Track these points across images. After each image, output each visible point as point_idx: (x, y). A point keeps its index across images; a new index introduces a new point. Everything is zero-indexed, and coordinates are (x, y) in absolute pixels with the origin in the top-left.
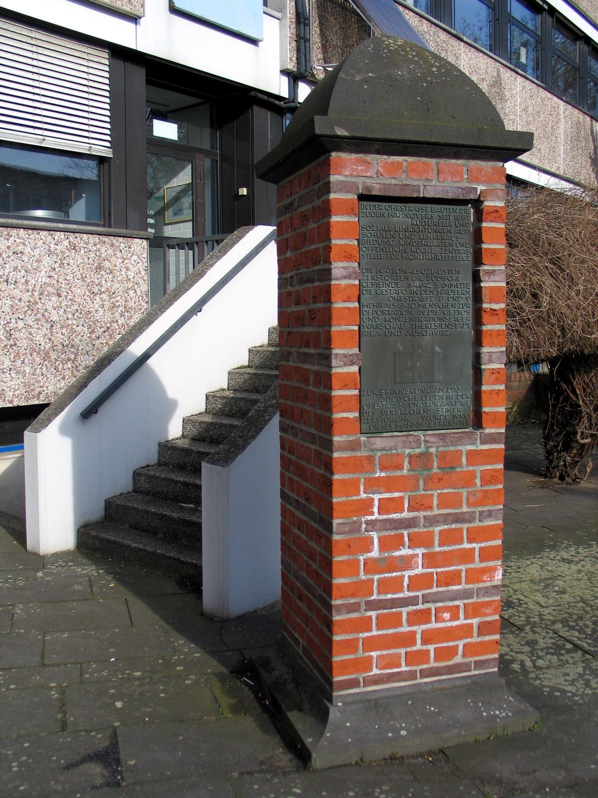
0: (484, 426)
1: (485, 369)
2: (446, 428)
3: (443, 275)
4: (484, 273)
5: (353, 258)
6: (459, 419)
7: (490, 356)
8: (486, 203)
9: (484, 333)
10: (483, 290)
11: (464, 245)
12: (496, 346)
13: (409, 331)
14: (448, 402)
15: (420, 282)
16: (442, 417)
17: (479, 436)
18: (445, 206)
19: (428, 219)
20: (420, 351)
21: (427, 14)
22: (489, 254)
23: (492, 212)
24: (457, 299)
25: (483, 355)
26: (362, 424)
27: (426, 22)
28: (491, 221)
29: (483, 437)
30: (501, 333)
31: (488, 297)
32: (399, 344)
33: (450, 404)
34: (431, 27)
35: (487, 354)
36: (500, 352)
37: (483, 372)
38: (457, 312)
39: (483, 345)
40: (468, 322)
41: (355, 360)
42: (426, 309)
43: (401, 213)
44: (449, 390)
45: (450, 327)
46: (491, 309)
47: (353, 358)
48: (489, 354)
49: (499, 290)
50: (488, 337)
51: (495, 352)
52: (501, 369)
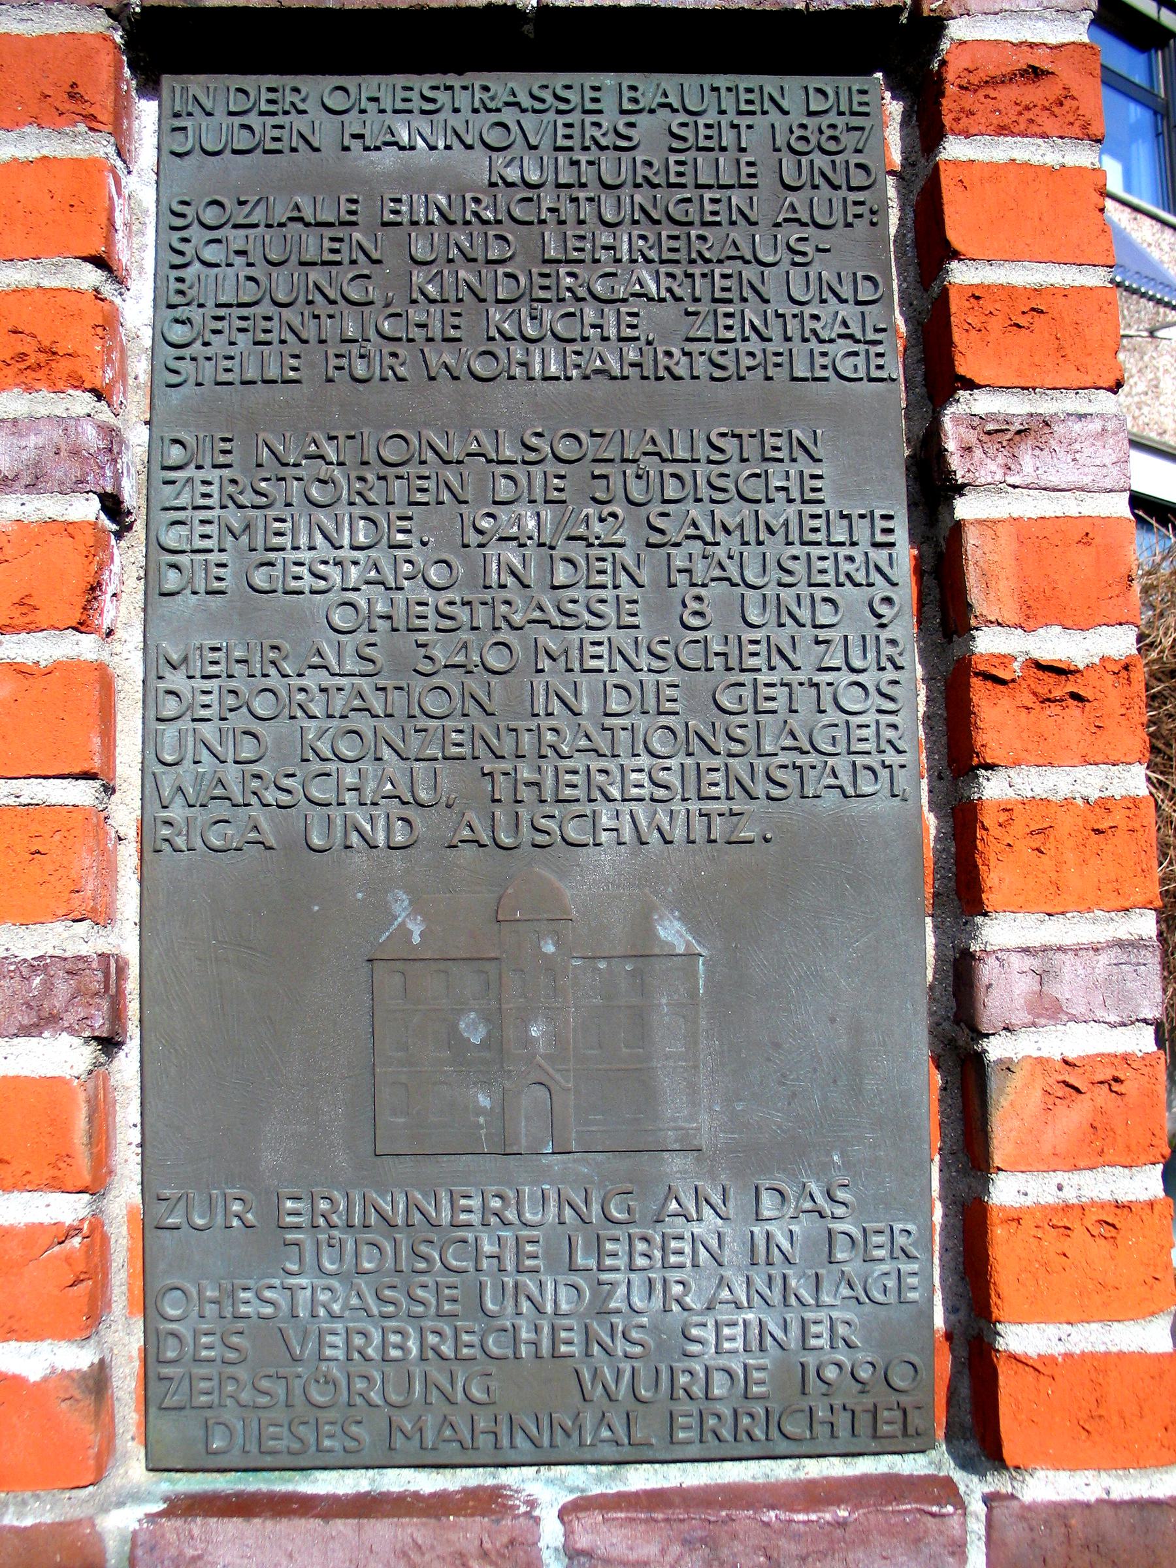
0: (1009, 1451)
1: (1008, 1067)
2: (750, 1449)
3: (702, 470)
4: (971, 437)
5: (63, 366)
6: (848, 1394)
7: (1042, 976)
8: (957, 29)
9: (989, 818)
10: (972, 539)
11: (846, 291)
12: (1085, 907)
13: (471, 816)
14: (760, 1283)
15: (547, 513)
16: (718, 1378)
17: (977, 1527)
18: (708, 80)
19: (594, 153)
20: (549, 948)
21: (1158, 207)
22: (996, 325)
23: (993, 82)
24: (804, 614)
25: (988, 971)
26: (153, 1410)
27: (1148, 222)
28: (1002, 130)
29: (1013, 1533)
30: (1118, 817)
31: (1005, 586)
32: (400, 904)
33: (776, 1297)
34: (1163, 232)
35: (1017, 962)
36: (1120, 944)
37: (994, 1082)
38: (804, 697)
39: (990, 899)
40: (891, 757)
41: (58, 1001)
42: (584, 680)
43: (422, 123)
44: (768, 1202)
45: (761, 788)
46: (1038, 665)
47: (48, 987)
48: (1029, 962)
49: (1086, 539)
50: (1024, 848)
51: (1077, 950)
52: (1126, 1058)
